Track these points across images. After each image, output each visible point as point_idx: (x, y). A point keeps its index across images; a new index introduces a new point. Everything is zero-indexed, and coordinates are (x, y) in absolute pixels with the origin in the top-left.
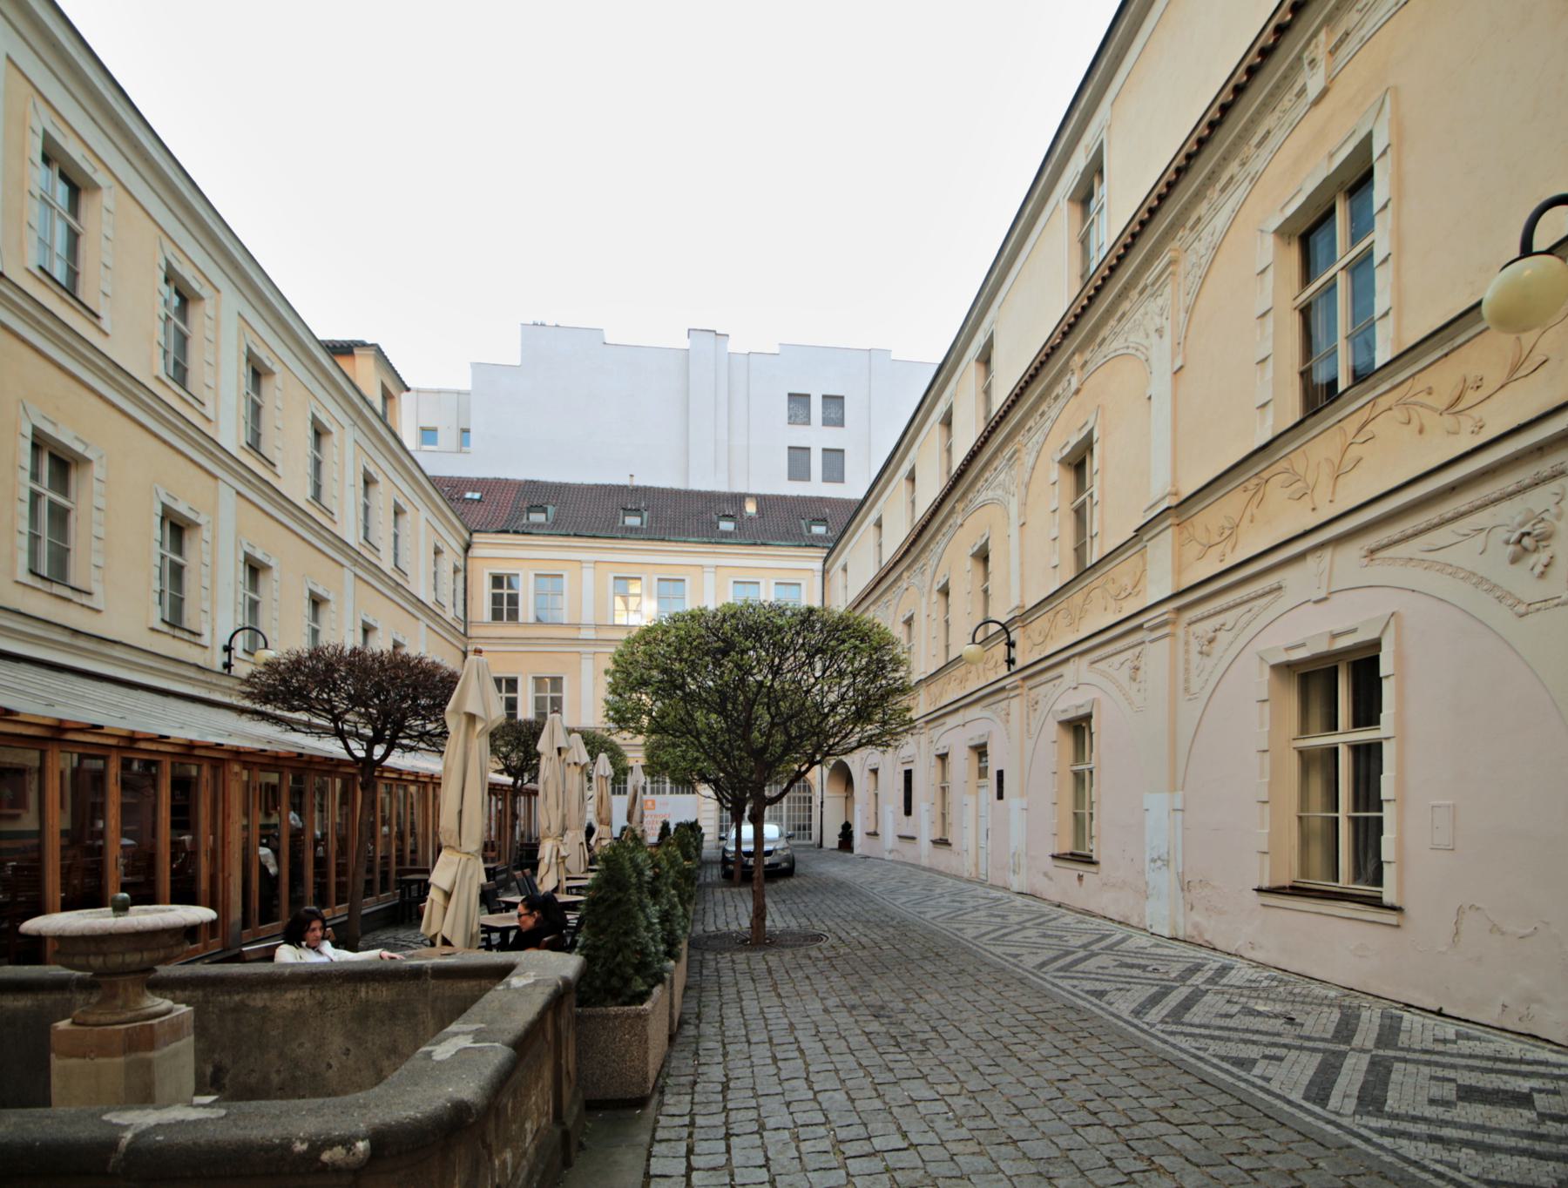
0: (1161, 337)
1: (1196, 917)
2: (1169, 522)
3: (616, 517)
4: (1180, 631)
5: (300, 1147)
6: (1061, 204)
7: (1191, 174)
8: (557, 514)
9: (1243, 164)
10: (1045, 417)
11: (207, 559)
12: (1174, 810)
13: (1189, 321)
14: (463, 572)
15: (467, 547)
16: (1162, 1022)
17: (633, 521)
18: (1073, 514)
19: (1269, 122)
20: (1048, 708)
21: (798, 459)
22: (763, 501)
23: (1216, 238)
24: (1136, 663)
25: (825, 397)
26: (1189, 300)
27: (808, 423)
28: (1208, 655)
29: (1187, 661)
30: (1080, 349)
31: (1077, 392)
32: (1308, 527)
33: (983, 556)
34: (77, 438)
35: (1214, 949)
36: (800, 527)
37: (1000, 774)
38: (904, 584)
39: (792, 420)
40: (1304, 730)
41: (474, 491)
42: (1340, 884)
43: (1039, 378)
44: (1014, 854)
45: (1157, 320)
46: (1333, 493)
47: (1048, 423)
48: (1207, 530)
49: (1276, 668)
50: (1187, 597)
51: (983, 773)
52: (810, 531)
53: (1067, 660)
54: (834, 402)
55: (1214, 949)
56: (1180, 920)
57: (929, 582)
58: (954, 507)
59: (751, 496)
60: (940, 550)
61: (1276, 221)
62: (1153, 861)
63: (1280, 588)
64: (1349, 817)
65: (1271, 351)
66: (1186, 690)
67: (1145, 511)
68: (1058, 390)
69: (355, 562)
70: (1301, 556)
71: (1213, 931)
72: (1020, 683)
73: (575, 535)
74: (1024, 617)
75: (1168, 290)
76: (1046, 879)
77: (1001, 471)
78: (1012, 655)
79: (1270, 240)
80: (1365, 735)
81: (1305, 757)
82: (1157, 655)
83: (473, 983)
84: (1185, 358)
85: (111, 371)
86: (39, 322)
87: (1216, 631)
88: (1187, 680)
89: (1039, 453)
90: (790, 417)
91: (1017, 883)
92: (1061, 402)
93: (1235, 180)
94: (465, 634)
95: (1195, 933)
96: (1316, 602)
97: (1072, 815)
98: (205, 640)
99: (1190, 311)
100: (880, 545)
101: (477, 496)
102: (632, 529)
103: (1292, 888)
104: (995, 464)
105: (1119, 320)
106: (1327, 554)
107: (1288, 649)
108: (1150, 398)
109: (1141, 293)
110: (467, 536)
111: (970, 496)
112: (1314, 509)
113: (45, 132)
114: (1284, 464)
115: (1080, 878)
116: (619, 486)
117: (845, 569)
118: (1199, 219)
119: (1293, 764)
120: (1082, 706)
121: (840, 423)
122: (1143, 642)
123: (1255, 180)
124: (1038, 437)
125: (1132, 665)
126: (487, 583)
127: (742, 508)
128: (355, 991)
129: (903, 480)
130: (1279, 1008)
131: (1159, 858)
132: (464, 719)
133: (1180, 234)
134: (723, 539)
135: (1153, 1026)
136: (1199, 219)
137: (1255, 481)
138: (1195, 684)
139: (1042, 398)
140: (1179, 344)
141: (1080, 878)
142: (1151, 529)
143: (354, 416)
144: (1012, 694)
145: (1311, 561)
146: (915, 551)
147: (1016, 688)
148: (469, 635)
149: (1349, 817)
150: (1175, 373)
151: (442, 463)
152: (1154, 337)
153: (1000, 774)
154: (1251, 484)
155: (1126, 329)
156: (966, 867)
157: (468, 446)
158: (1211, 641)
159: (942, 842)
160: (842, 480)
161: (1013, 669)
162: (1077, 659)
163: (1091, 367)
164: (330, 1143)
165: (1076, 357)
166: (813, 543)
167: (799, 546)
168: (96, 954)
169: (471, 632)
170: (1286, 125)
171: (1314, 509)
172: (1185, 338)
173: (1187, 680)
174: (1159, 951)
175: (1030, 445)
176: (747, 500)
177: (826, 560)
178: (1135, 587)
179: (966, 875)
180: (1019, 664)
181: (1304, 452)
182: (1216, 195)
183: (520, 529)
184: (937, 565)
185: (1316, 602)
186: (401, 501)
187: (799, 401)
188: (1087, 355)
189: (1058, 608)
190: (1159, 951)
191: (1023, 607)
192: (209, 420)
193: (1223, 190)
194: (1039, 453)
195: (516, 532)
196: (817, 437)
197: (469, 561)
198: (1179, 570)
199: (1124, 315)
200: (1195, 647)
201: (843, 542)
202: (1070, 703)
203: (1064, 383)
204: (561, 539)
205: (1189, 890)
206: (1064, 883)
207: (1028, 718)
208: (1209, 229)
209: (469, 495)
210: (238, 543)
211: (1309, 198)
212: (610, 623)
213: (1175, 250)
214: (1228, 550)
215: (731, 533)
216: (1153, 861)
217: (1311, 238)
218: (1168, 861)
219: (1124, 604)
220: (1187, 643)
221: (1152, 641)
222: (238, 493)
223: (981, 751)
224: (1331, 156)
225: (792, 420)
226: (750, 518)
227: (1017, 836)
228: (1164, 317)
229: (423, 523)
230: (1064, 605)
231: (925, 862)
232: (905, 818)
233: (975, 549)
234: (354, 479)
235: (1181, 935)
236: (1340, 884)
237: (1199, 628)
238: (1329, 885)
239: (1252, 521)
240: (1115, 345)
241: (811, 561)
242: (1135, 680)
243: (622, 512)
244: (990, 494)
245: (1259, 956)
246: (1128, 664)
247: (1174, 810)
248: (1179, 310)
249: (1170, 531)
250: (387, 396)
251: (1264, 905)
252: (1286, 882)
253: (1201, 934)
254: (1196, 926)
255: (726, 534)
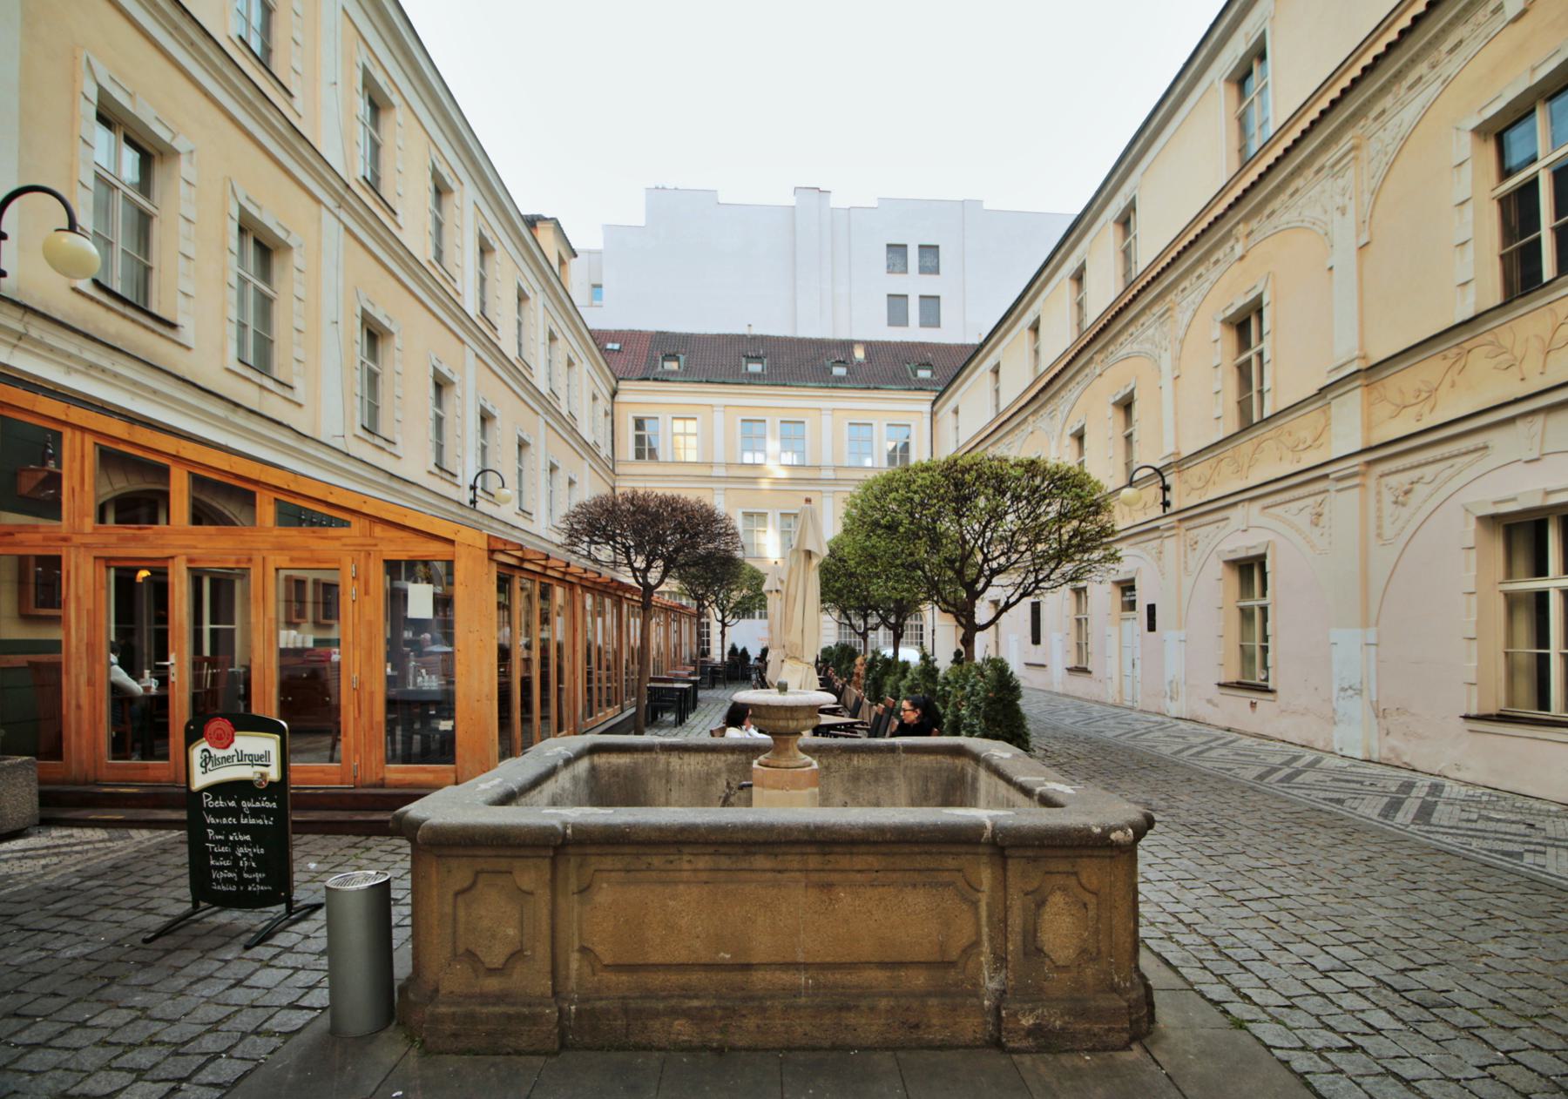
0: (1343, 214)
1: (1393, 741)
2: (1358, 383)
3: (739, 364)
4: (1371, 482)
5: (1097, 830)
6: (1216, 82)
7: (1376, 74)
8: (687, 361)
9: (1433, 67)
10: (1202, 280)
11: (459, 412)
12: (1367, 644)
13: (1375, 203)
14: (611, 415)
15: (614, 393)
16: (1412, 823)
17: (755, 368)
18: (1235, 371)
19: (1460, 32)
20: (1212, 546)
21: (897, 302)
22: (869, 346)
23: (1405, 129)
24: (1319, 510)
25: (921, 247)
26: (1374, 183)
27: (905, 271)
28: (1404, 505)
29: (1379, 509)
30: (1246, 219)
31: (1242, 258)
32: (1519, 395)
33: (1126, 405)
34: (386, 316)
35: (1414, 770)
36: (906, 371)
37: (1151, 609)
38: (1028, 428)
39: (891, 269)
40: (1510, 575)
41: (613, 342)
42: (1553, 712)
43: (1198, 244)
44: (1171, 682)
45: (1339, 200)
46: (1544, 365)
47: (1207, 285)
48: (1401, 392)
49: (1482, 520)
50: (1377, 453)
51: (1131, 606)
52: (916, 375)
53: (1235, 504)
54: (930, 252)
55: (1414, 770)
56: (1375, 744)
57: (1060, 426)
58: (1092, 358)
59: (858, 342)
60: (1073, 397)
61: (1476, 121)
62: (1343, 690)
63: (1486, 448)
64: (1562, 654)
65: (1469, 236)
66: (1379, 536)
67: (1330, 372)
68: (1219, 254)
69: (547, 412)
70: (1511, 420)
71: (1412, 753)
72: (1176, 524)
73: (707, 382)
74: (1180, 464)
75: (1350, 173)
76: (1210, 706)
77: (1149, 327)
78: (1167, 498)
79: (1467, 138)
80: (1262, 602)
81: (1512, 601)
82: (1343, 505)
83: (932, 757)
84: (1371, 235)
85: (407, 259)
86: (366, 223)
87: (1412, 483)
88: (1379, 527)
89: (1195, 312)
90: (888, 267)
91: (1174, 709)
92: (1222, 267)
93: (1424, 80)
94: (613, 471)
95: (1391, 756)
96: (1527, 462)
97: (1238, 648)
98: (459, 481)
99: (1376, 193)
100: (997, 391)
101: (616, 346)
102: (755, 375)
103: (1498, 715)
104: (1142, 320)
105: (1292, 195)
106: (1539, 420)
107: (1495, 503)
108: (1331, 269)
109: (1318, 172)
110: (614, 383)
111: (1111, 348)
112: (1522, 379)
113: (364, 66)
114: (1488, 337)
115: (1253, 705)
116: (739, 336)
117: (956, 412)
118: (1384, 112)
119: (1500, 605)
120: (1254, 547)
121: (936, 270)
122: (1327, 491)
123: (1447, 83)
124: (1193, 297)
125: (1314, 511)
126: (631, 425)
127: (851, 354)
128: (850, 759)
129: (1026, 329)
130: (1519, 817)
131: (1350, 687)
132: (803, 555)
133: (1362, 123)
134: (837, 383)
135: (1407, 826)
136: (1384, 112)
137: (1455, 351)
138: (1388, 532)
139: (1200, 261)
140: (1365, 223)
141: (1253, 705)
142: (1337, 389)
143: (544, 283)
144: (1167, 534)
145: (1521, 426)
146: (1043, 398)
147: (1172, 528)
148: (617, 471)
149: (1562, 654)
150: (1361, 248)
151: (597, 320)
152: (1337, 216)
153: (1151, 609)
154: (1452, 353)
155: (1300, 203)
156: (1111, 694)
157: (601, 299)
158: (1407, 493)
159: (1080, 670)
160: (938, 325)
161: (1168, 511)
162: (1246, 504)
163: (1257, 236)
164: (1113, 829)
165: (1241, 226)
166: (921, 387)
167: (909, 390)
168: (793, 719)
169: (617, 470)
170: (1483, 35)
171: (1522, 379)
172: (1371, 217)
173: (1379, 527)
174: (1353, 769)
175: (1184, 304)
176: (856, 346)
177: (934, 403)
178: (1315, 440)
179: (1110, 701)
180: (1174, 507)
181: (1511, 328)
182: (1402, 92)
183: (660, 377)
184: (1070, 411)
185: (1527, 462)
186: (572, 355)
187: (897, 251)
188: (1254, 224)
189: (1221, 456)
190: (1353, 769)
191: (1178, 454)
192: (458, 294)
193: (1411, 88)
194: (1195, 312)
195: (656, 380)
196: (914, 284)
197: (616, 406)
198: (1368, 427)
199: (1297, 191)
200: (1388, 498)
201: (955, 386)
202: (1244, 546)
203: (1227, 247)
204: (696, 385)
205: (1385, 717)
206: (1236, 709)
207: (1185, 556)
208: (1396, 120)
209: (610, 346)
210: (477, 397)
211: (1509, 104)
212: (739, 461)
213: (1357, 137)
214: (1427, 409)
215: (844, 378)
216: (1343, 690)
217: (1505, 135)
218: (1361, 691)
219: (1304, 455)
220: (1379, 493)
221: (1339, 491)
222: (477, 355)
223: (1127, 587)
224: (1534, 70)
225: (891, 269)
226: (859, 364)
227: (1174, 665)
228: (1347, 196)
229: (585, 374)
230: (1229, 453)
231: (1058, 688)
232: (1033, 647)
233: (1118, 398)
234: (542, 337)
235: (1375, 757)
236: (1553, 712)
237: (1393, 481)
238: (1543, 715)
239: (1453, 386)
240: (1285, 218)
241: (919, 404)
242: (1317, 525)
243: (744, 360)
244: (1136, 347)
245: (1468, 777)
246: (1308, 510)
247: (1367, 644)
248: (1362, 192)
249: (1358, 391)
250: (562, 262)
251: (1471, 731)
252: (1493, 710)
253: (1398, 757)
254: (1392, 749)
255: (840, 379)
